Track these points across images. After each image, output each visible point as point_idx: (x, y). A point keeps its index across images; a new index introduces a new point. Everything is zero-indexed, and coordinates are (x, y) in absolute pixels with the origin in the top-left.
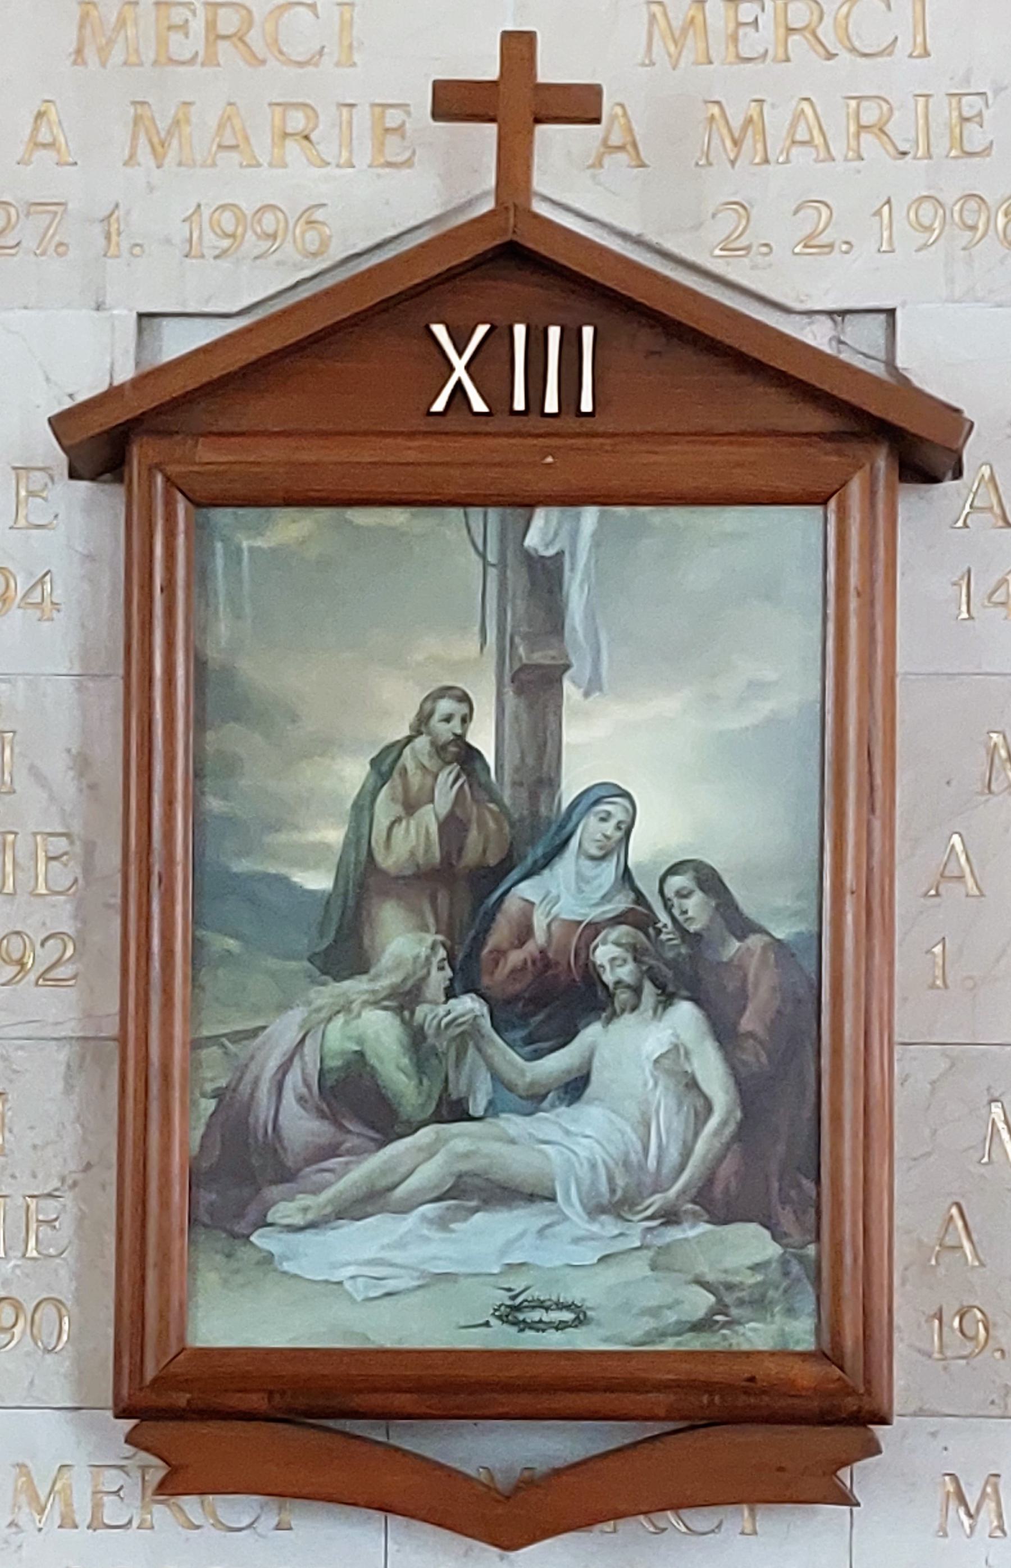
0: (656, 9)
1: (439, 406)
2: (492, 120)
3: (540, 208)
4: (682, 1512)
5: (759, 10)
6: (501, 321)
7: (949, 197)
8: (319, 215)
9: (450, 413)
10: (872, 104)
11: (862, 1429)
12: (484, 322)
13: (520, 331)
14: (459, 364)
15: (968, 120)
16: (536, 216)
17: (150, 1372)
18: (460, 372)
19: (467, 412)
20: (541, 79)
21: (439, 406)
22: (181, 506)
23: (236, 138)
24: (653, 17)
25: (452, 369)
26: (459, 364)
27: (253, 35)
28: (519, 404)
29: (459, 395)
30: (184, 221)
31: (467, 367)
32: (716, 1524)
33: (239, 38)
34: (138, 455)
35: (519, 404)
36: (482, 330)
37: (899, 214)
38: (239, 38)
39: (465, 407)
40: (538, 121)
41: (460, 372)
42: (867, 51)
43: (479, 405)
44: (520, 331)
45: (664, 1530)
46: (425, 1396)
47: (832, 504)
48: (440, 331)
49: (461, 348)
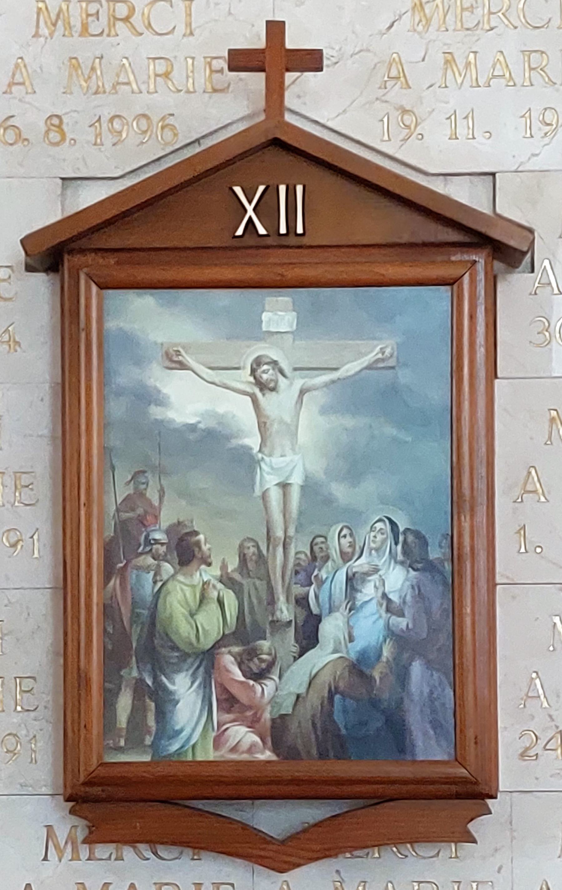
0: (41, 5)
1: (240, 232)
2: (263, 70)
3: (289, 118)
4: (416, 845)
5: (99, 6)
6: (291, 183)
7: (129, 116)
8: (11, 122)
9: (246, 236)
10: (538, 55)
11: (481, 801)
12: (262, 184)
13: (282, 189)
14: (250, 208)
15: (534, 69)
16: (289, 125)
17: (82, 779)
18: (250, 212)
19: (256, 235)
20: (289, 45)
21: (240, 232)
22: (94, 288)
23: (23, 78)
24: (40, 9)
25: (246, 211)
26: (250, 208)
27: (136, 20)
28: (283, 230)
29: (250, 225)
30: (90, 126)
31: (254, 210)
32: (436, 852)
33: (126, 20)
34: (67, 261)
35: (283, 230)
36: (261, 188)
37: (105, 126)
38: (126, 20)
39: (255, 231)
40: (288, 70)
41: (250, 212)
42: (160, 32)
43: (262, 231)
44: (282, 189)
45: (406, 856)
46: (390, 785)
47: (455, 287)
48: (238, 190)
49: (250, 199)
